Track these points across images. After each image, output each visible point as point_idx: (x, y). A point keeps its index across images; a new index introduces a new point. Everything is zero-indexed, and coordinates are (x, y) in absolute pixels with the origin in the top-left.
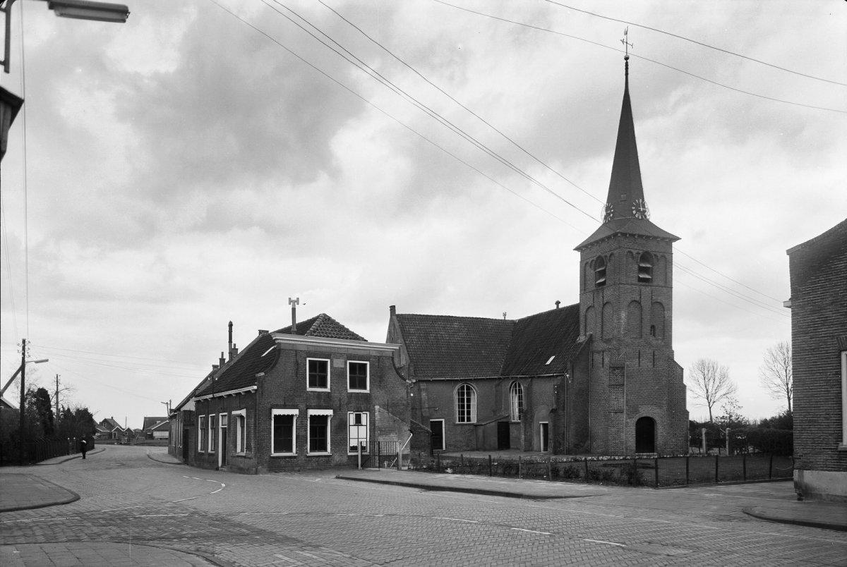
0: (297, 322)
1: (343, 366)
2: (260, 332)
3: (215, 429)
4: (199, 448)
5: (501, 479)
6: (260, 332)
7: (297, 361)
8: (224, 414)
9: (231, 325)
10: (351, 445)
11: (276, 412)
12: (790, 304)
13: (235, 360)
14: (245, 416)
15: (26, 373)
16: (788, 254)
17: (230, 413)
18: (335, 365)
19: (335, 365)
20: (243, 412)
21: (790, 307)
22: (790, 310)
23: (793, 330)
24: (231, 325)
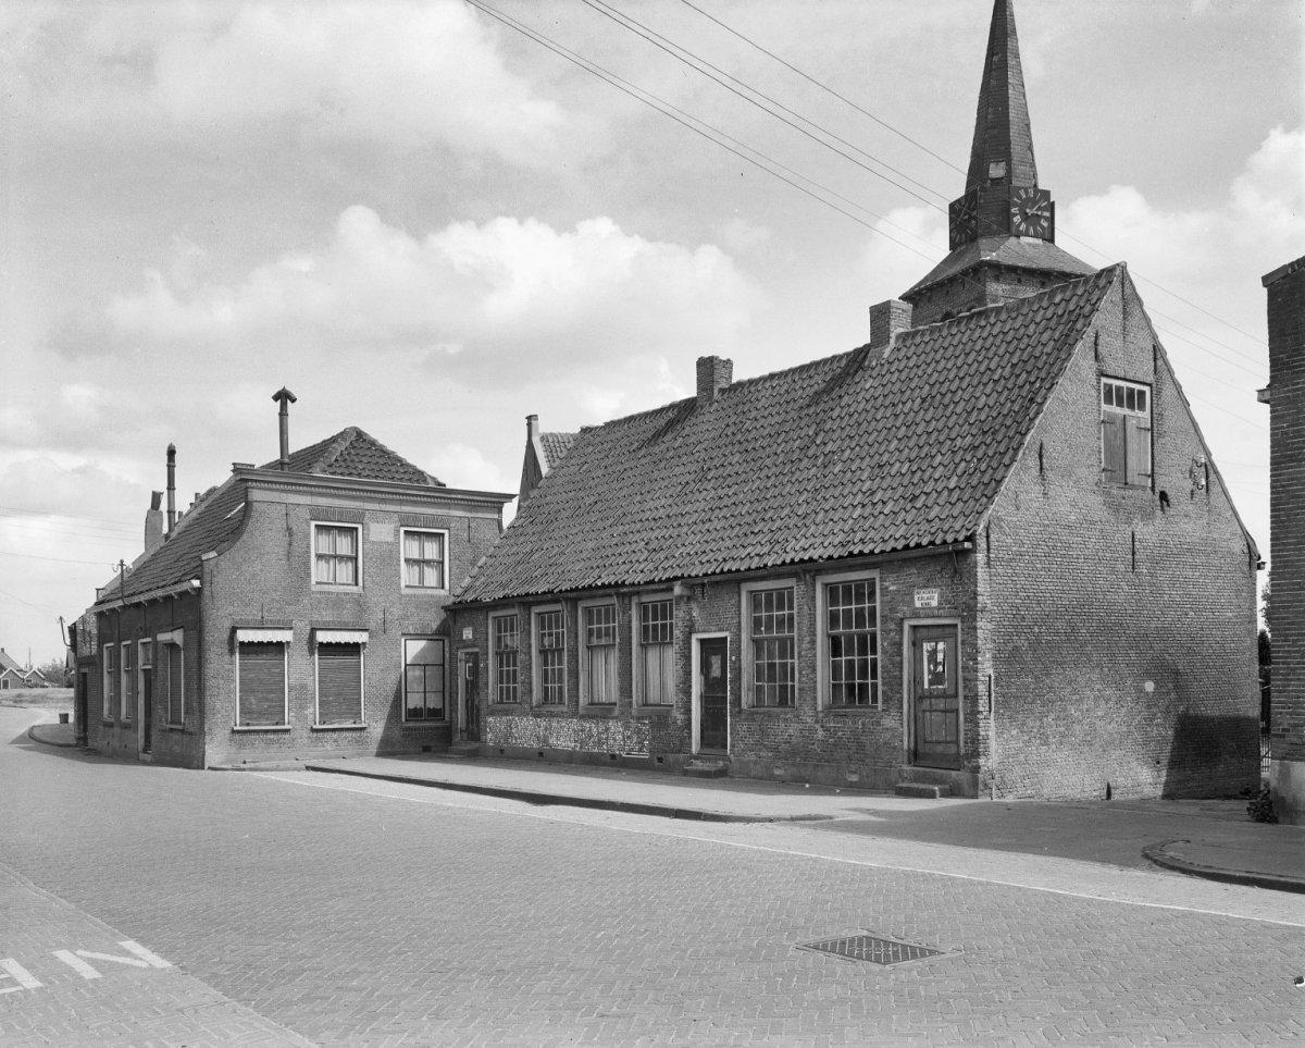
0: (290, 452)
1: (391, 539)
2: (559, 235)
3: (132, 674)
4: (106, 712)
5: (1096, 869)
6: (559, 235)
7: (289, 529)
8: (145, 640)
9: (171, 453)
10: (411, 706)
11: (926, 686)
12: (1267, 396)
13: (177, 530)
14: (181, 646)
15: (1228, 886)
16: (1264, 286)
17: (155, 638)
18: (373, 538)
19: (373, 538)
20: (177, 637)
21: (1266, 402)
22: (1268, 406)
23: (1272, 452)
24: (171, 453)
